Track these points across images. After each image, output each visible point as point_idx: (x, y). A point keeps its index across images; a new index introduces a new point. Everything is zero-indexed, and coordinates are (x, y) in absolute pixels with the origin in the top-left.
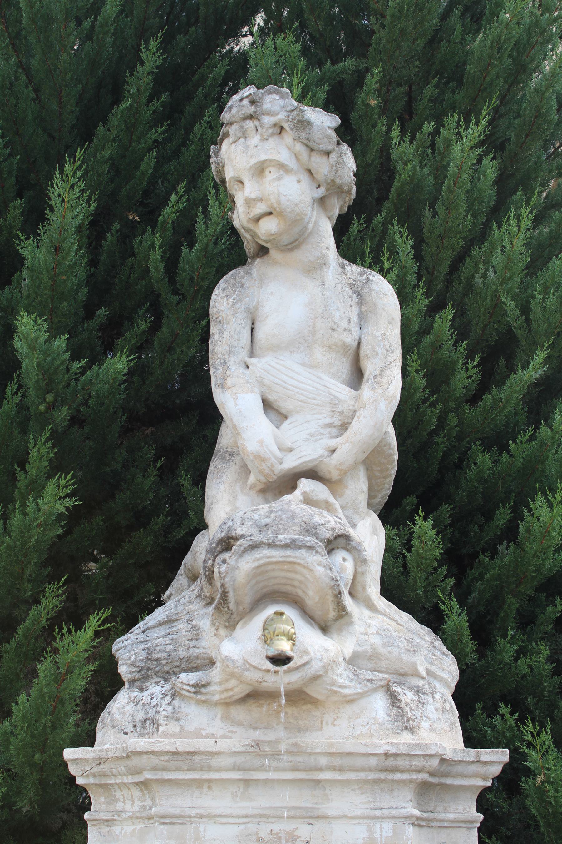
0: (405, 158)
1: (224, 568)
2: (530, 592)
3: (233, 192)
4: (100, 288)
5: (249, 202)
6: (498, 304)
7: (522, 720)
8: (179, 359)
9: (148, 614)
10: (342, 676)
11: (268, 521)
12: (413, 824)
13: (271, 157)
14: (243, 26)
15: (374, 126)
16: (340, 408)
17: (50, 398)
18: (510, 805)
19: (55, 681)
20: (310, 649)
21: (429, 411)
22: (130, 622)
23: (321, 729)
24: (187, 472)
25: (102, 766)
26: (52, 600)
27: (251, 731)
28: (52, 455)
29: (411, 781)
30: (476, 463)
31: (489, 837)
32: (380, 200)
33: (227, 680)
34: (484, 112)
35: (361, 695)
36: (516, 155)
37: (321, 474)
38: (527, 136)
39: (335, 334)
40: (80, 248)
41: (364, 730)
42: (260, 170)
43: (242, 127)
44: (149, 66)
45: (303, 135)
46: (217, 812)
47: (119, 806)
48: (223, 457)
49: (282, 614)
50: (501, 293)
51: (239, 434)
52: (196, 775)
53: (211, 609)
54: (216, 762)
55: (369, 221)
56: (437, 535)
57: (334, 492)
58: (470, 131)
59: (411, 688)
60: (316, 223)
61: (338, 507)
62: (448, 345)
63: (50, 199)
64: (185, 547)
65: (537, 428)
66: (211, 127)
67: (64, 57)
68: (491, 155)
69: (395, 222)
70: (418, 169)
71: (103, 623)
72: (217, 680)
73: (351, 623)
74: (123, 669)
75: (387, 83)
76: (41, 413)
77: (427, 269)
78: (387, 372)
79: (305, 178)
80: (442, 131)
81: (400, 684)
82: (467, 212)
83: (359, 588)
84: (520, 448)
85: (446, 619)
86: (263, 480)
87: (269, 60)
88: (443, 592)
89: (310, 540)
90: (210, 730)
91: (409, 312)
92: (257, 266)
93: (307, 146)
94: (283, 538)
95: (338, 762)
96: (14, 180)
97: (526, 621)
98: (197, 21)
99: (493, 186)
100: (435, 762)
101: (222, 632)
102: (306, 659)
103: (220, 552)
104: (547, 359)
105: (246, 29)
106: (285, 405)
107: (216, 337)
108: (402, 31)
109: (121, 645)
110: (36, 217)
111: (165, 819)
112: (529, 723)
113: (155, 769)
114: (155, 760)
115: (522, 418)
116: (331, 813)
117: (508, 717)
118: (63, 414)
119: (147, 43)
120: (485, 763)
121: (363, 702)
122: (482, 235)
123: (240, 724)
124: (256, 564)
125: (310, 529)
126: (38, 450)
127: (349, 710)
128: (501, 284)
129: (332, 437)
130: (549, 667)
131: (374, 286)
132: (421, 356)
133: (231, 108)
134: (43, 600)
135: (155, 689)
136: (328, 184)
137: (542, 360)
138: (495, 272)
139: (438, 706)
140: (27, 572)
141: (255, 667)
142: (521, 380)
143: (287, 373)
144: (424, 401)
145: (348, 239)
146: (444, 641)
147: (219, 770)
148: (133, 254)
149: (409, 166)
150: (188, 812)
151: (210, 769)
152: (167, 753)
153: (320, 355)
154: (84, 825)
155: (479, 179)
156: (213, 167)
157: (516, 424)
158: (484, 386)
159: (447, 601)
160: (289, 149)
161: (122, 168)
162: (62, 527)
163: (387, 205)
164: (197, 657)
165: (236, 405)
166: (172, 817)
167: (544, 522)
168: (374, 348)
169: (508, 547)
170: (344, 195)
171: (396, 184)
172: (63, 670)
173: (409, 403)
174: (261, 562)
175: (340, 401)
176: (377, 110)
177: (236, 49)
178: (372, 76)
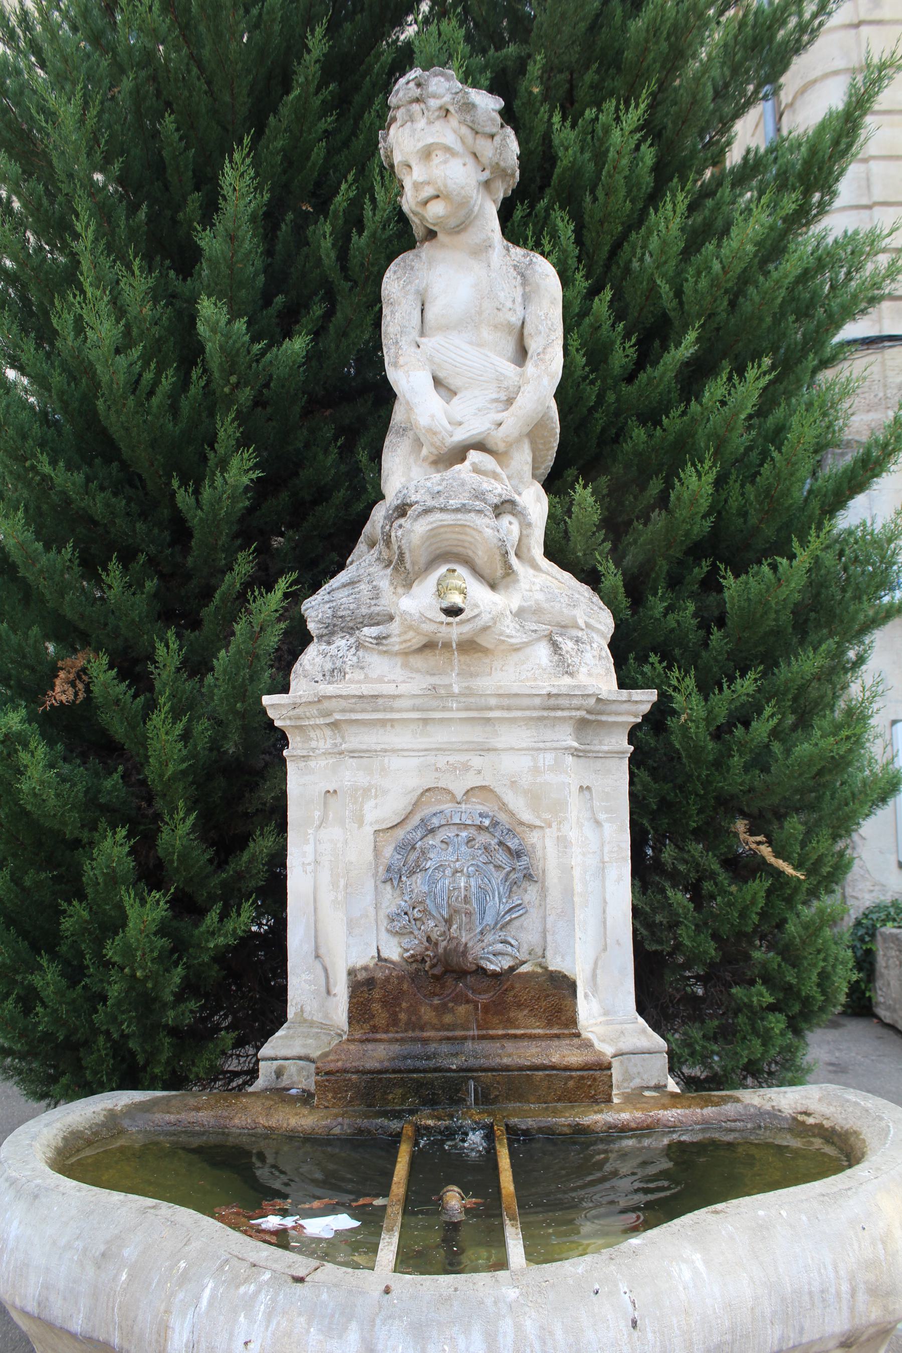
0: (566, 144)
1: (400, 533)
2: (679, 555)
3: (401, 176)
4: (276, 279)
5: (417, 186)
6: (653, 288)
7: (669, 667)
8: (354, 344)
9: (332, 577)
10: (509, 628)
11: (440, 488)
12: (572, 755)
13: (437, 140)
14: (407, 15)
15: (537, 113)
16: (505, 384)
17: (233, 379)
18: (657, 741)
19: (251, 638)
20: (480, 603)
21: (588, 388)
22: (315, 587)
23: (490, 674)
24: (364, 449)
25: (297, 710)
26: (244, 565)
27: (428, 677)
28: (238, 434)
29: (571, 718)
30: (631, 438)
31: (638, 768)
32: (542, 189)
33: (405, 632)
34: (643, 96)
35: (527, 644)
36: (672, 142)
37: (489, 446)
38: (683, 123)
39: (500, 314)
40: (254, 236)
41: (529, 674)
42: (427, 153)
43: (409, 111)
44: (316, 53)
45: (468, 118)
46: (400, 747)
47: (314, 744)
48: (397, 432)
49: (454, 571)
50: (656, 276)
51: (411, 409)
52: (380, 716)
53: (389, 571)
54: (397, 704)
55: (532, 206)
56: (596, 501)
57: (500, 463)
58: (630, 116)
59: (571, 639)
60: (481, 206)
61: (505, 477)
62: (607, 326)
63: (222, 188)
64: (364, 517)
65: (688, 401)
66: (378, 116)
67: (233, 46)
68: (649, 142)
69: (556, 207)
70: (578, 154)
71: (290, 586)
72: (396, 632)
73: (518, 581)
74: (311, 626)
75: (549, 70)
76: (226, 395)
77: (587, 254)
78: (549, 350)
79: (470, 160)
80: (600, 116)
81: (561, 635)
82: (626, 197)
83: (525, 550)
84: (673, 422)
85: (603, 579)
86: (436, 452)
87: (432, 47)
88: (600, 555)
89: (479, 505)
90: (391, 677)
91: (571, 294)
92: (426, 250)
93: (472, 129)
94: (454, 503)
95: (506, 702)
96: (190, 174)
97: (675, 582)
98: (362, 10)
99: (651, 172)
100: (592, 701)
101: (400, 590)
102: (476, 612)
103: (397, 518)
104: (698, 340)
105: (410, 18)
106: (454, 382)
107: (388, 318)
108: (563, 16)
109: (309, 605)
110: (211, 207)
111: (354, 753)
112: (676, 669)
113: (343, 711)
114: (343, 703)
115: (674, 395)
116: (499, 746)
117: (657, 665)
118: (246, 395)
119: (313, 31)
120: (636, 702)
121: (528, 650)
122: (638, 221)
123: (418, 671)
124: (430, 527)
125: (479, 495)
126: (225, 430)
127: (516, 657)
128: (657, 268)
129: (499, 412)
130: (694, 622)
131: (537, 268)
132: (581, 336)
133: (398, 91)
134: (236, 567)
135: (341, 642)
136: (492, 167)
137: (693, 339)
138: (651, 256)
139: (595, 653)
140: (220, 543)
141: (430, 620)
142: (674, 358)
143: (457, 351)
144: (585, 378)
145: (512, 225)
146: (602, 598)
147: (400, 711)
148: (308, 244)
149: (570, 151)
150: (374, 747)
151: (392, 710)
152: (354, 696)
153: (487, 334)
154: (283, 761)
155: (637, 165)
156: (382, 152)
157: (669, 401)
158: (640, 365)
159: (604, 562)
160: (455, 132)
161: (293, 159)
162: (248, 499)
163: (548, 191)
164: (378, 614)
165: (408, 382)
166: (360, 752)
167: (693, 491)
168: (537, 327)
169: (660, 513)
170: (508, 178)
171: (558, 171)
172: (257, 629)
173: (570, 380)
174: (434, 525)
175: (505, 377)
176: (539, 98)
177: (402, 38)
178: (535, 62)
